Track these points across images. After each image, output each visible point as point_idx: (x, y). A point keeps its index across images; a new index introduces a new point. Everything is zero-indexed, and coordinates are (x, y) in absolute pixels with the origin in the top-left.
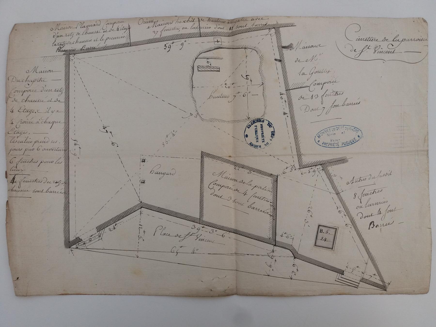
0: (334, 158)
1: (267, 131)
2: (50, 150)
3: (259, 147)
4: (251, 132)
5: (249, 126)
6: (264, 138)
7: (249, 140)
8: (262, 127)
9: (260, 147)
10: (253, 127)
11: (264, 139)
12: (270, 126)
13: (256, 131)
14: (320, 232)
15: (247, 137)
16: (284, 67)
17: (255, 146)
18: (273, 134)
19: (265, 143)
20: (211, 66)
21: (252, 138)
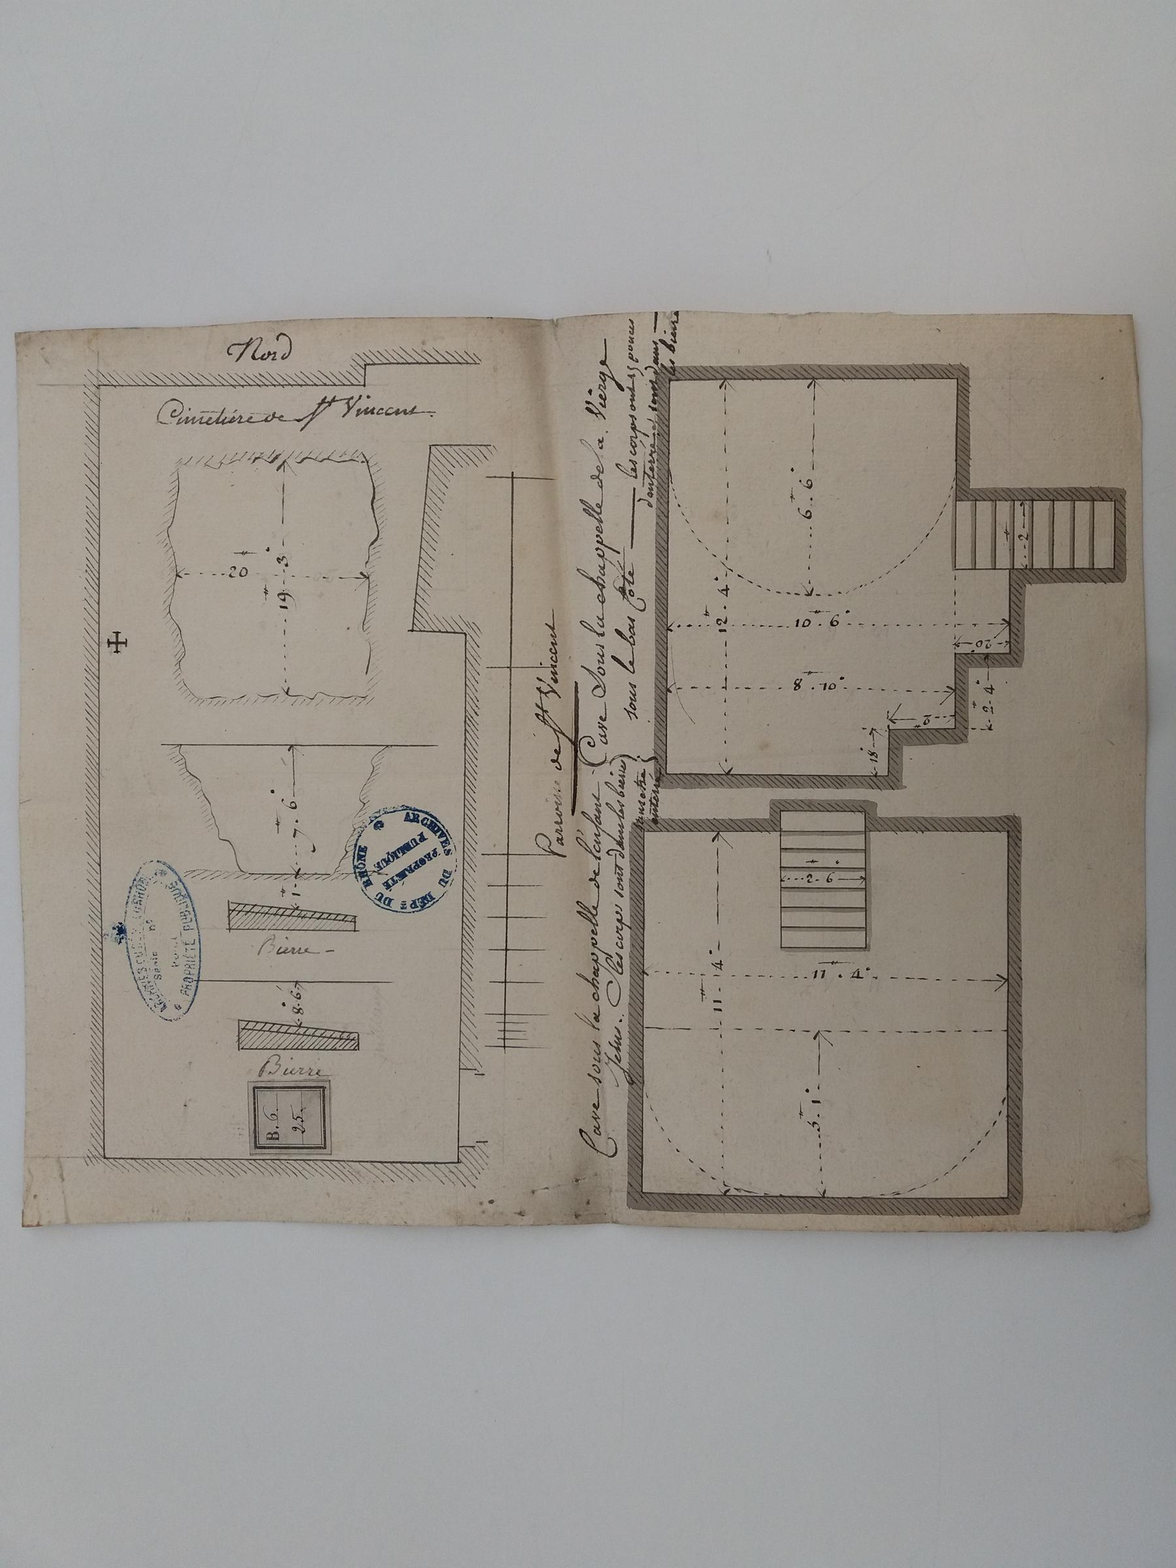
0: (974, 313)
1: (422, 882)
2: (397, 413)
3: (365, 879)
4: (400, 831)
5: (412, 817)
6: (400, 883)
7: (369, 837)
8: (430, 857)
9: (368, 883)
10: (415, 829)
11: (395, 882)
12: (381, 898)
13: (406, 848)
14: (278, 1139)
15: (376, 827)
16: (1102, 576)
17: (361, 866)
18: (425, 901)
19: (387, 894)
20: (600, 826)
21: (378, 845)
